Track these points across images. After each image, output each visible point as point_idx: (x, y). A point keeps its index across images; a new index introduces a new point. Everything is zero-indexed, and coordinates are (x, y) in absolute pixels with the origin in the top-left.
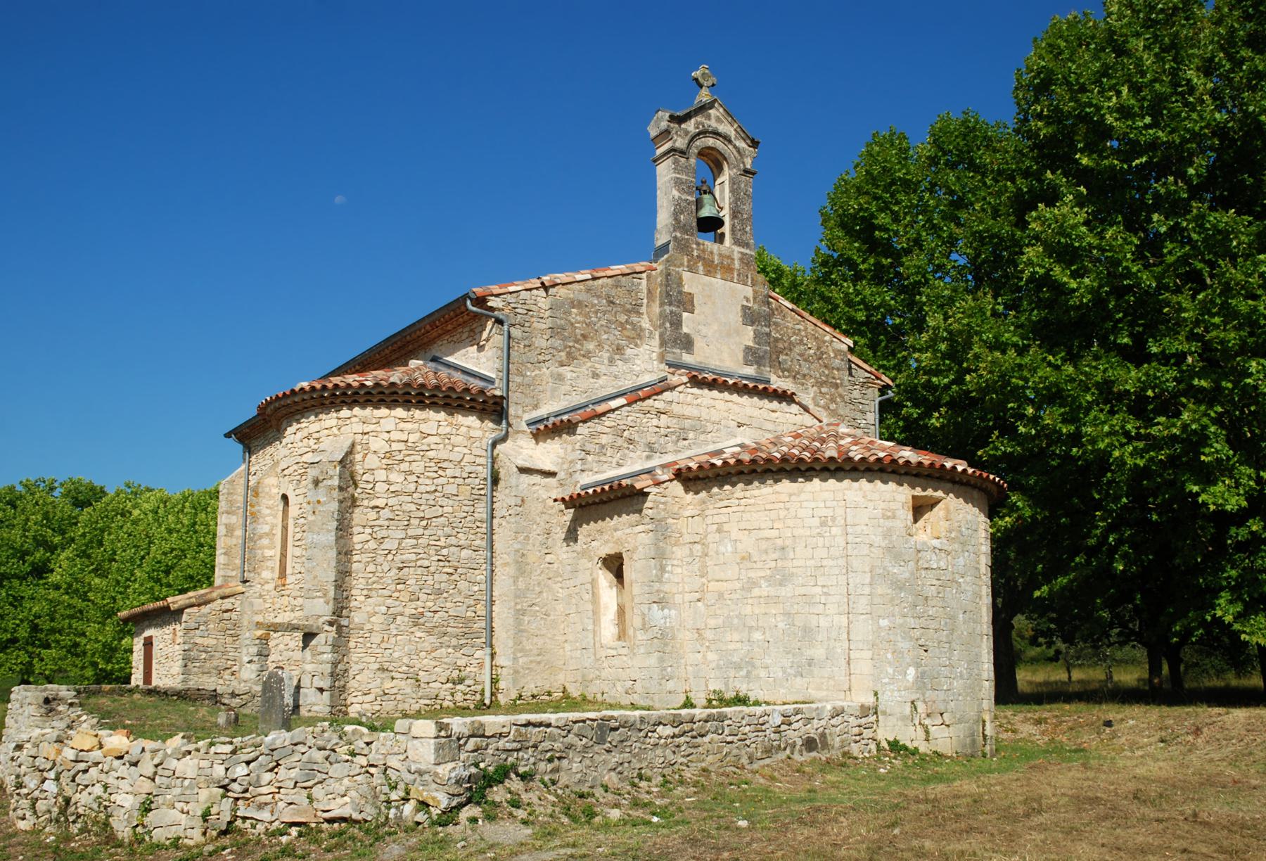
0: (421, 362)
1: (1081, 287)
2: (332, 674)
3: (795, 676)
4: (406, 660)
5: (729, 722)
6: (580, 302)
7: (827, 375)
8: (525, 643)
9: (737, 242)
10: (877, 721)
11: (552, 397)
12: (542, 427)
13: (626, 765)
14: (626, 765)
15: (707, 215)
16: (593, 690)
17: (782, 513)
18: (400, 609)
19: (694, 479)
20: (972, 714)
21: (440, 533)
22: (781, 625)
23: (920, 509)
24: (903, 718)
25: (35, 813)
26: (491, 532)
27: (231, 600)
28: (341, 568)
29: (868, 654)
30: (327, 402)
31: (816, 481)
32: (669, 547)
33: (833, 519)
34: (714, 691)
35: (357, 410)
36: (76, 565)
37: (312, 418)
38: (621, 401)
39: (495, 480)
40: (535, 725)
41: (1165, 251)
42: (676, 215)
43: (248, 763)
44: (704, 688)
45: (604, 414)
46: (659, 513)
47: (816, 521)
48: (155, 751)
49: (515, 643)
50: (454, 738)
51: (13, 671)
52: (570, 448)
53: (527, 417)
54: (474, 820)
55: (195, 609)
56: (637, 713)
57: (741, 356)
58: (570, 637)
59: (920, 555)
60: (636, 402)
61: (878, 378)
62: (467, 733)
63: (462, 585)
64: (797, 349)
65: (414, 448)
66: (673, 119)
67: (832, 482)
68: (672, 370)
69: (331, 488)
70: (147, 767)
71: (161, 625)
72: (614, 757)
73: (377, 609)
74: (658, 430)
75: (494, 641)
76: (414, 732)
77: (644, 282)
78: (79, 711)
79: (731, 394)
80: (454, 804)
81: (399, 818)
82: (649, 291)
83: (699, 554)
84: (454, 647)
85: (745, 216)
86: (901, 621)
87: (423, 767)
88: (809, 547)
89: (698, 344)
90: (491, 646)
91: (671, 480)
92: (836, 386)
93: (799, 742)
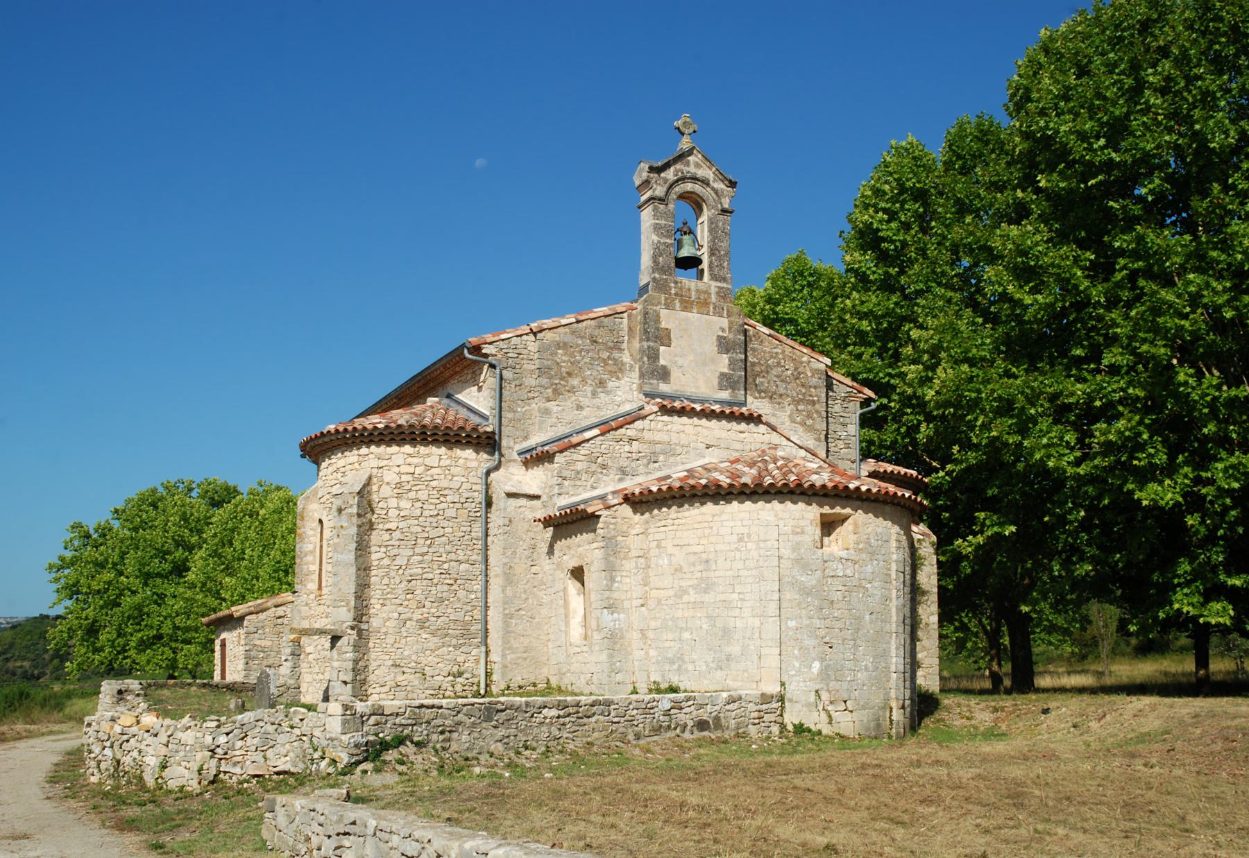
0: (437, 399)
1: (1033, 301)
2: (353, 670)
4: (414, 657)
5: (617, 706)
6: (565, 344)
7: (804, 394)
8: (512, 641)
9: (714, 277)
10: (783, 708)
11: (540, 429)
12: (529, 457)
13: (512, 738)
14: (512, 738)
15: (686, 255)
16: (564, 683)
17: (707, 531)
18: (409, 615)
19: (641, 502)
20: (877, 700)
21: (442, 550)
23: (829, 526)
24: (808, 705)
25: (100, 770)
27: (283, 608)
28: (360, 582)
30: (350, 442)
31: (735, 503)
32: (618, 561)
33: (749, 535)
34: (654, 682)
35: (373, 448)
36: (209, 565)
37: (340, 455)
38: (596, 432)
39: (489, 504)
40: (428, 707)
41: (1117, 267)
42: (655, 258)
43: (227, 734)
44: (646, 679)
45: (579, 444)
46: (609, 532)
47: (735, 538)
48: (169, 727)
49: (504, 643)
50: (358, 716)
51: (161, 667)
52: (550, 474)
53: (518, 447)
54: (365, 772)
55: (254, 616)
56: (524, 699)
57: (716, 382)
58: (552, 637)
60: (609, 431)
63: (461, 594)
64: (774, 372)
65: (419, 479)
66: (652, 169)
67: (748, 503)
68: (648, 399)
69: (351, 515)
70: (163, 738)
71: (230, 630)
73: (391, 615)
75: (489, 641)
76: (329, 712)
77: (625, 321)
79: (700, 419)
80: (353, 761)
81: (317, 770)
82: (630, 329)
84: (454, 646)
85: (723, 253)
86: (808, 622)
87: (333, 736)
89: (675, 374)
90: (486, 645)
91: (620, 504)
92: (813, 403)
93: (690, 723)
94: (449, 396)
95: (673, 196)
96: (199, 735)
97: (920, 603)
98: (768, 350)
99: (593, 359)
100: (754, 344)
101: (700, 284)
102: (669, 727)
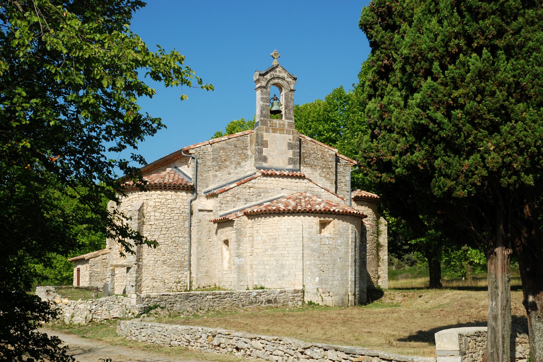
0: (171, 169)
4: (160, 276)
6: (223, 148)
8: (201, 269)
9: (287, 118)
10: (304, 295)
11: (213, 183)
16: (221, 286)
17: (275, 227)
18: (159, 259)
19: (251, 215)
20: (343, 292)
21: (172, 232)
24: (314, 294)
26: (190, 231)
27: (106, 255)
31: (286, 217)
33: (291, 229)
38: (235, 184)
39: (192, 214)
40: (165, 295)
45: (228, 190)
47: (286, 230)
48: (74, 303)
53: (204, 190)
54: (144, 317)
55: (93, 259)
56: (200, 292)
57: (287, 162)
58: (217, 267)
62: (145, 297)
63: (180, 250)
64: (313, 156)
65: (163, 204)
66: (260, 75)
67: (291, 217)
69: (135, 219)
70: (72, 307)
71: (82, 264)
77: (249, 138)
78: (56, 294)
79: (279, 178)
82: (251, 141)
84: (177, 271)
89: (269, 159)
90: (190, 270)
92: (330, 168)
93: (264, 301)
94: (176, 167)
95: (269, 85)
96: (86, 305)
97: (380, 250)
99: (235, 153)
100: (303, 145)
101: (281, 122)
102: (256, 302)
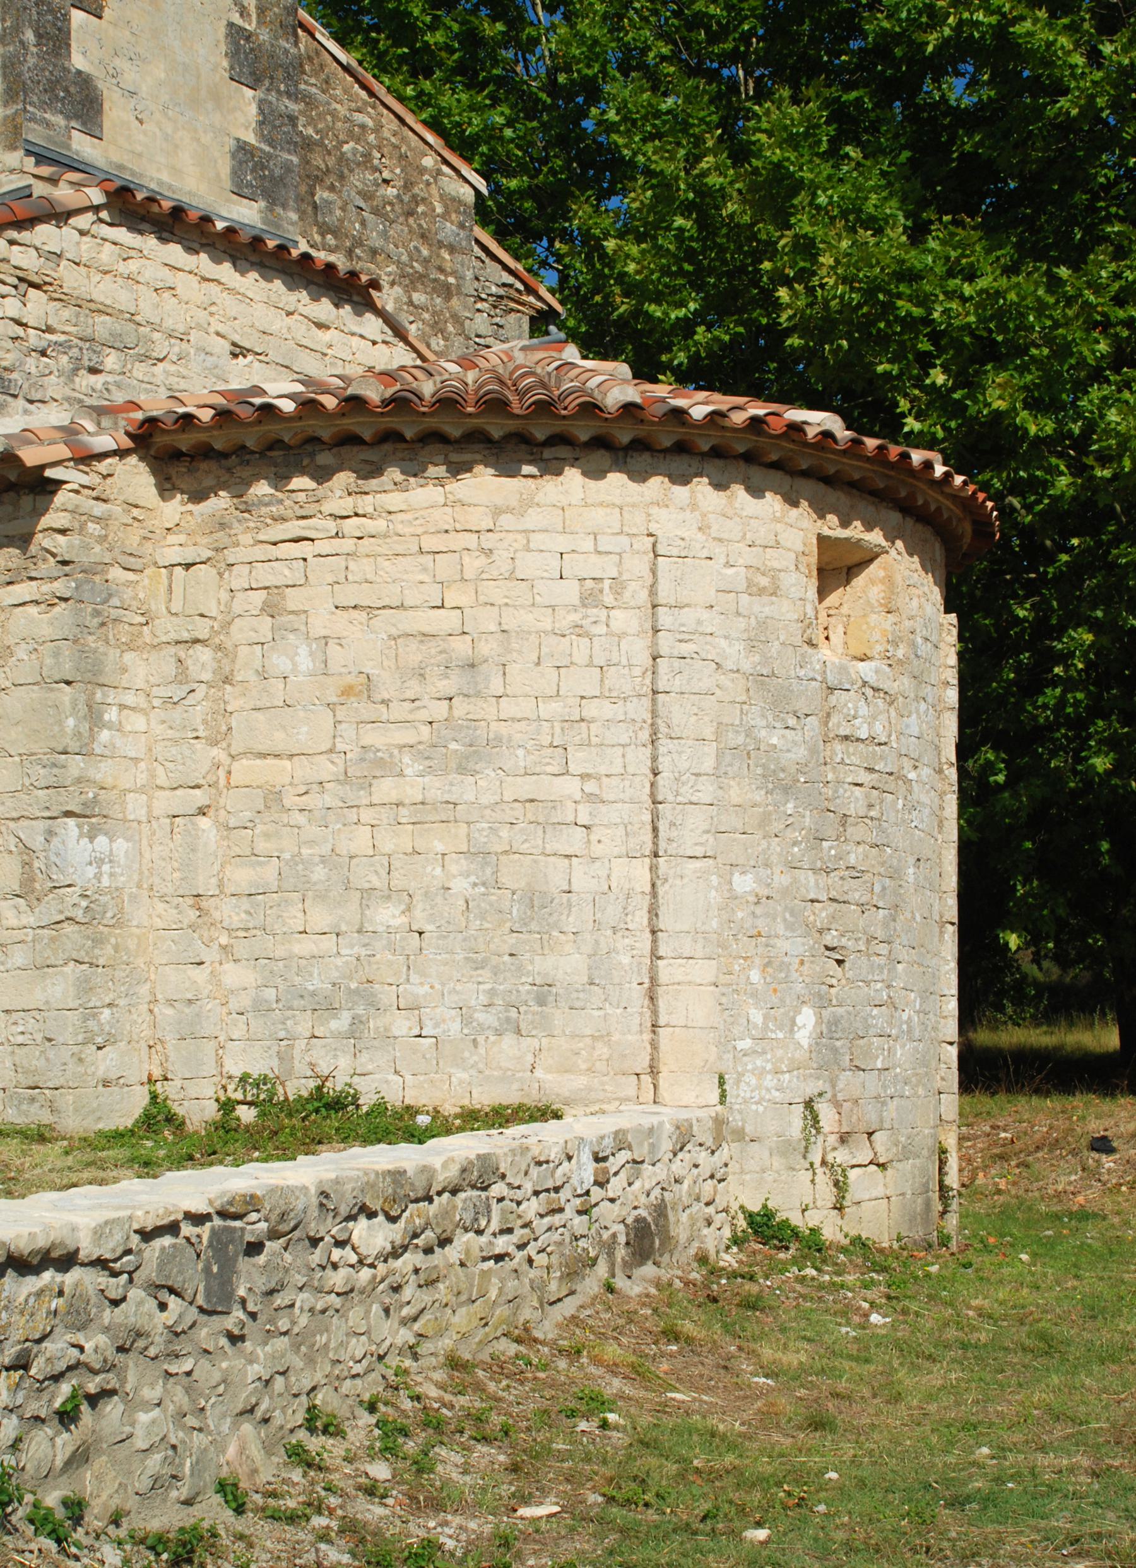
3: (499, 1033)
7: (426, 261)
22: (460, 885)
29: (704, 971)
31: (572, 476)
34: (244, 1079)
44: (210, 1068)
46: (87, 548)
47: (570, 592)
57: (225, 167)
59: (833, 699)
61: (530, 290)
64: (360, 179)
67: (616, 480)
68: (46, 171)
72: (251, 1360)
74: (20, 331)
83: (206, 676)
86: (785, 880)
88: (547, 663)
91: (121, 453)
92: (447, 292)
98: (342, 110)
